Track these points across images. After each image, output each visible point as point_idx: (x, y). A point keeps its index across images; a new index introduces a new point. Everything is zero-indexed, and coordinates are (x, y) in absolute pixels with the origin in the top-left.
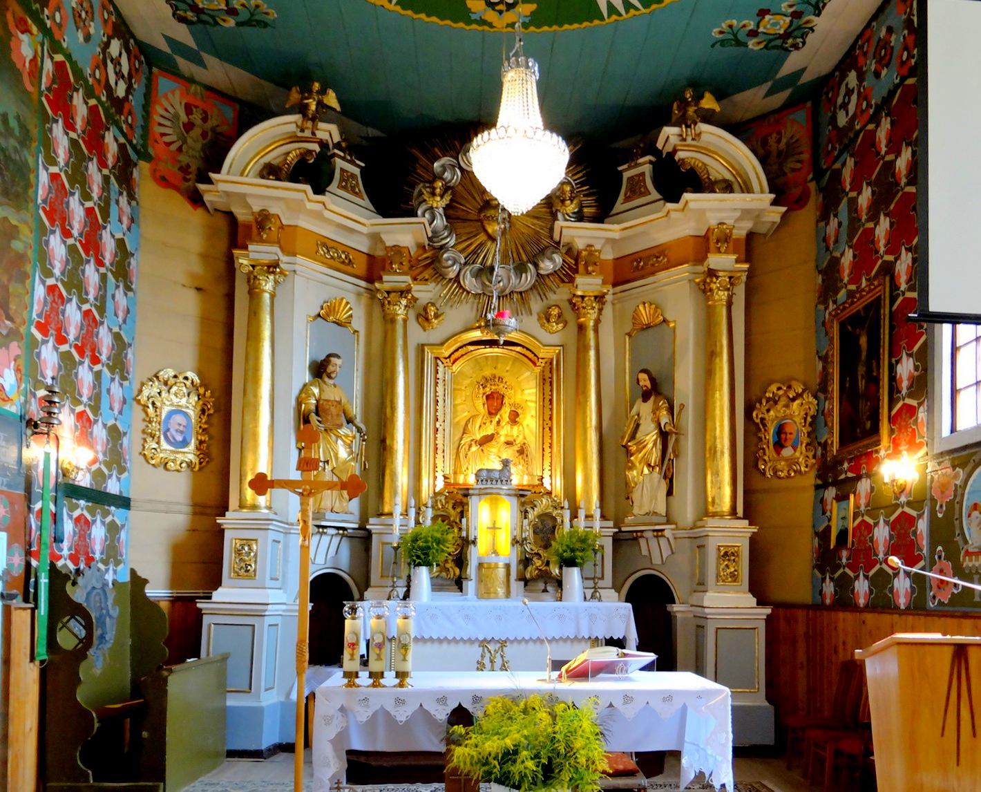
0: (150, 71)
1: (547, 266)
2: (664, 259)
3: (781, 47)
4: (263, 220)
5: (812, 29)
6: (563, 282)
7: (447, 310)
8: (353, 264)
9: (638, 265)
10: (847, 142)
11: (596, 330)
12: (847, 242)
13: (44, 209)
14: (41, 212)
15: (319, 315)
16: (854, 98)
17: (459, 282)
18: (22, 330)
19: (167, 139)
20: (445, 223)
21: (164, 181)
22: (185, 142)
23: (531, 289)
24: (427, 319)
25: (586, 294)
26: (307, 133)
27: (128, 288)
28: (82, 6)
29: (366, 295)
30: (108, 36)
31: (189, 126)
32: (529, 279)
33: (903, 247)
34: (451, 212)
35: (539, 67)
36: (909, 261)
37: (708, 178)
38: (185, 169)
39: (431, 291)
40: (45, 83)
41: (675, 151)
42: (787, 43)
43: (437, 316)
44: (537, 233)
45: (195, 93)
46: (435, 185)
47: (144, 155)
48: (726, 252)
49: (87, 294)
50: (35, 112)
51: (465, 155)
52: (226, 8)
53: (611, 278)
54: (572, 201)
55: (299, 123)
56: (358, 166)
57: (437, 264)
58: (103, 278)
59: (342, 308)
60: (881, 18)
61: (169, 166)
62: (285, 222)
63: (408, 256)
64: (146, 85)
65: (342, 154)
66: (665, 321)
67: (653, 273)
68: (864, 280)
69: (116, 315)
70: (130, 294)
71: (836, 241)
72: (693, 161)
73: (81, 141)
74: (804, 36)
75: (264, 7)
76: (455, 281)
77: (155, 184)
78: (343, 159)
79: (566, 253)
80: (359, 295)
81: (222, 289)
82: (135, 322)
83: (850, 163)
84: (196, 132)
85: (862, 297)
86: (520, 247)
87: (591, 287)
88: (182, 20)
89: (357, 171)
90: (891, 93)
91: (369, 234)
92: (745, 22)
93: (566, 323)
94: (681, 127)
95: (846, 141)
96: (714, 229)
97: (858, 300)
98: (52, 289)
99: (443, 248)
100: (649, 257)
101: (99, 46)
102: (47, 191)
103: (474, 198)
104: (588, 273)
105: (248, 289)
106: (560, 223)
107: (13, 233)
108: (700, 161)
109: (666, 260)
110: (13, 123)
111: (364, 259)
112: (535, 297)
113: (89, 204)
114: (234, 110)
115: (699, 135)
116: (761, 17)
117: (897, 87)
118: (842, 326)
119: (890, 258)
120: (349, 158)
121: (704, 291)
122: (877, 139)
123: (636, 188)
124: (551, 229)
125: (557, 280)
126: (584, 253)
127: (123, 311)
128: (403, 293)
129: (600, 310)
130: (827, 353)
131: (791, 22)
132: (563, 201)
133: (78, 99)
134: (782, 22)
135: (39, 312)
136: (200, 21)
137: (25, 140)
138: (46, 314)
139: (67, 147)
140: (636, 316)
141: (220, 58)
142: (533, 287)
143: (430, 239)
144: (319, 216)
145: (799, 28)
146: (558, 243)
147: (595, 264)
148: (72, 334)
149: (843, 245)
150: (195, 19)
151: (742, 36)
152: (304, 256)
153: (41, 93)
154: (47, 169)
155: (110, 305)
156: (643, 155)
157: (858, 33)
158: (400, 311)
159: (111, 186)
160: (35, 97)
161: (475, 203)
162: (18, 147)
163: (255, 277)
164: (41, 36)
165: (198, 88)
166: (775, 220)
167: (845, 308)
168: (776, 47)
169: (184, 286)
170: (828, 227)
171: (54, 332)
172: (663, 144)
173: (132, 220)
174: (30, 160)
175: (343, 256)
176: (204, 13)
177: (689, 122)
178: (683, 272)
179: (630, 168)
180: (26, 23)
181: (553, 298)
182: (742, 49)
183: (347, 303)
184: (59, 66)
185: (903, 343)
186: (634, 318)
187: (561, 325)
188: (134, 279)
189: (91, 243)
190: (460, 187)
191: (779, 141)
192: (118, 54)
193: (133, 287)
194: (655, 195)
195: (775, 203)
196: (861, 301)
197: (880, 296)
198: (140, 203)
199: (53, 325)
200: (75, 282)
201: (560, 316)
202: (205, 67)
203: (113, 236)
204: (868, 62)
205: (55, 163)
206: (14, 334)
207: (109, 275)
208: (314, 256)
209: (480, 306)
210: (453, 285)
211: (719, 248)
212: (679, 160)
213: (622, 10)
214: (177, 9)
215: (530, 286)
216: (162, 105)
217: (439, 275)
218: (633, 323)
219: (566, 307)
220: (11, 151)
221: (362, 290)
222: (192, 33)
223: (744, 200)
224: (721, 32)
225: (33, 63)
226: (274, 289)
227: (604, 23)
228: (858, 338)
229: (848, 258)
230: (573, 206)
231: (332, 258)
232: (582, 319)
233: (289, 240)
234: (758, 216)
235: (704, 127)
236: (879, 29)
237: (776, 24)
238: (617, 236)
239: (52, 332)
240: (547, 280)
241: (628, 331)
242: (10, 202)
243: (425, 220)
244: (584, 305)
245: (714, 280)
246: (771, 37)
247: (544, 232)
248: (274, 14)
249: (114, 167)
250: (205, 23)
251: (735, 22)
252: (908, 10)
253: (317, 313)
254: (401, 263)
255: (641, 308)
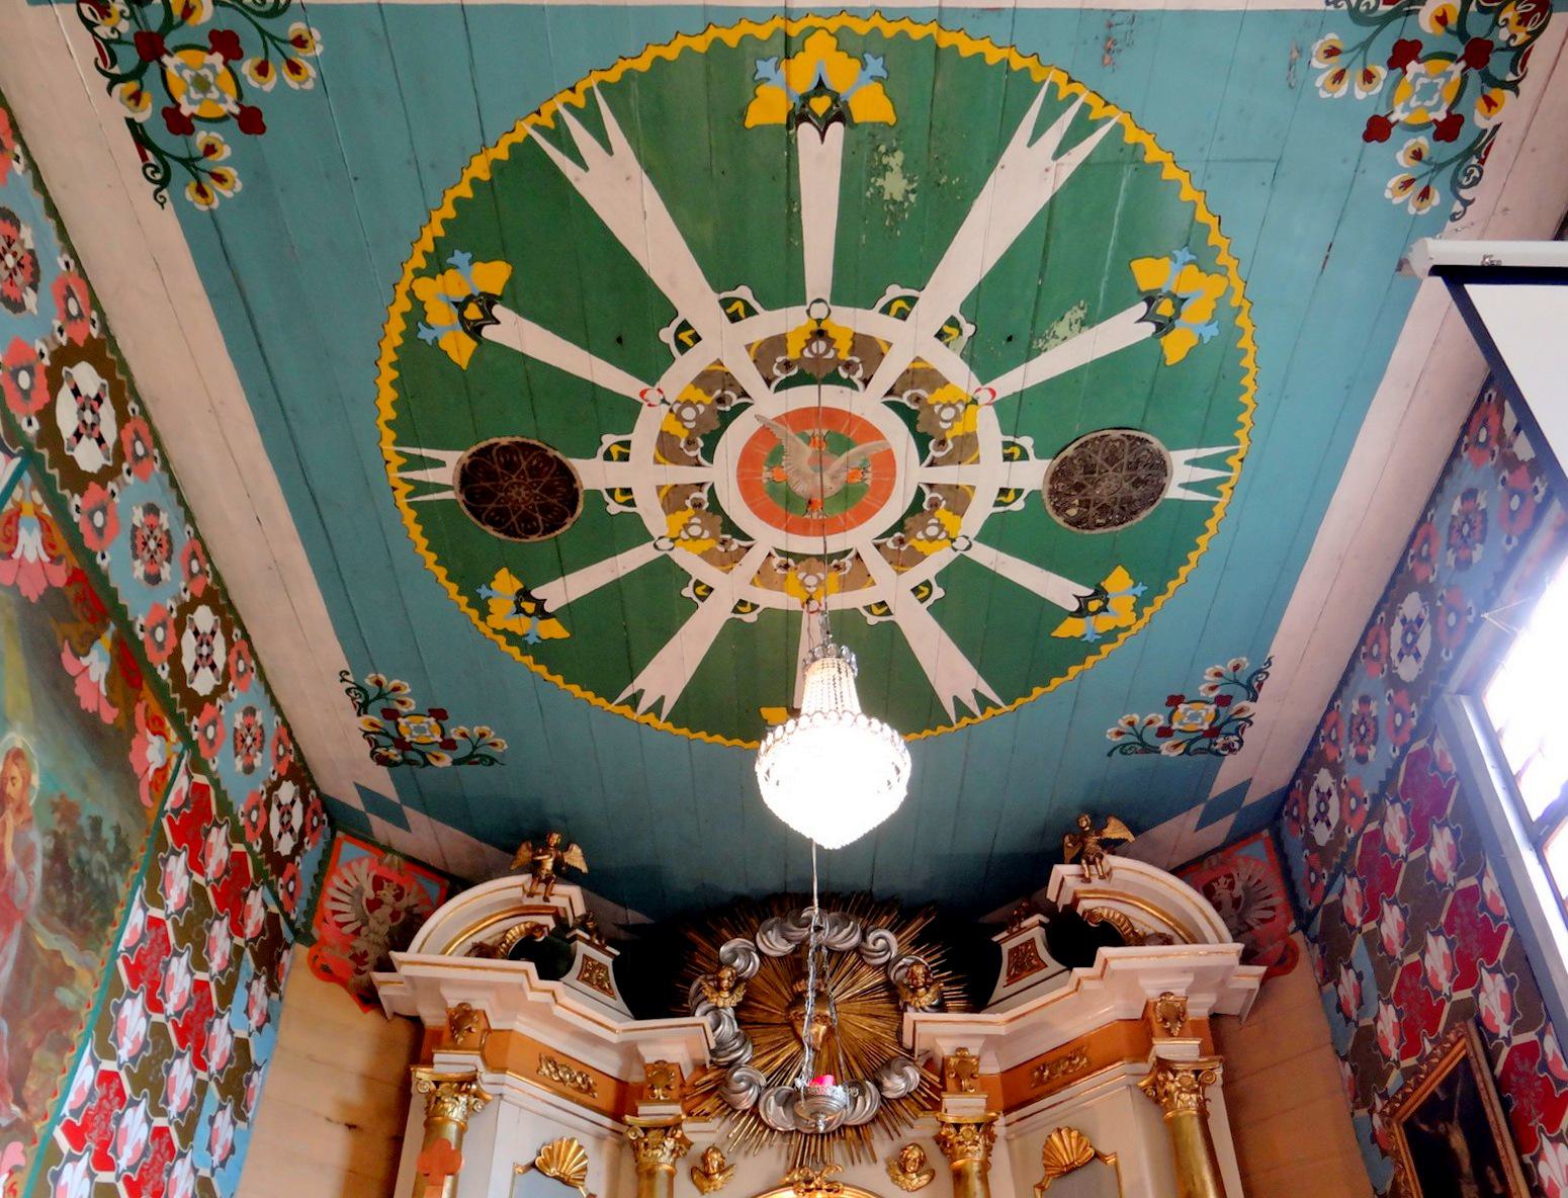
0: (333, 835)
1: (896, 1085)
2: (1081, 1060)
3: (1209, 750)
4: (461, 1018)
5: (1248, 720)
6: (924, 1109)
7: (740, 1160)
8: (594, 1091)
9: (1041, 1075)
10: (1339, 860)
11: (984, 1178)
12: (1379, 998)
13: (126, 961)
14: (120, 963)
15: (533, 1165)
16: (1334, 801)
17: (758, 1116)
18: (37, 1127)
19: (340, 918)
20: (737, 1030)
21: (325, 973)
22: (365, 923)
23: (872, 1121)
24: (707, 1175)
25: (962, 1121)
26: (537, 901)
27: (240, 1114)
28: (249, 730)
29: (610, 1138)
30: (279, 775)
31: (374, 904)
32: (868, 1104)
33: (1484, 972)
34: (745, 1014)
35: (857, 657)
36: (1503, 987)
37: (1133, 931)
38: (359, 958)
39: (713, 1132)
40: (173, 803)
41: (1076, 901)
42: (1216, 744)
43: (722, 1170)
44: (877, 1038)
45: (389, 866)
46: (721, 975)
47: (303, 935)
48: (1181, 1036)
49: (167, 1102)
50: (147, 832)
51: (765, 933)
52: (440, 740)
53: (1001, 1103)
54: (928, 990)
55: (527, 887)
56: (610, 954)
57: (724, 1089)
58: (201, 1088)
59: (570, 1155)
60: (1346, 693)
61: (337, 953)
62: (493, 1026)
63: (679, 1076)
64: (324, 851)
65: (587, 937)
66: (1097, 1155)
67: (1067, 1084)
68: (1426, 1043)
69: (210, 1148)
70: (241, 1125)
71: (1360, 1003)
72: (1106, 911)
73: (209, 890)
74: (1239, 731)
75: (491, 737)
76: (751, 1114)
77: (311, 974)
78: (589, 943)
79: (924, 1067)
80: (600, 1138)
81: (386, 1128)
82: (240, 1170)
83: (1353, 886)
84: (384, 912)
85: (1432, 1068)
86: (851, 1059)
87: (966, 1111)
88: (383, 761)
89: (608, 961)
90: (1392, 773)
91: (622, 1043)
92: (1151, 716)
93: (933, 1175)
94: (1079, 863)
95: (1336, 860)
96: (1156, 1003)
97: (1428, 1075)
98: (107, 1078)
99: (732, 1065)
100: (1057, 1063)
101: (264, 783)
102: (138, 937)
103: (779, 992)
104: (961, 1090)
105: (424, 1118)
106: (911, 1015)
107: (66, 975)
108: (1116, 911)
109: (1085, 1060)
110: (107, 833)
111: (611, 1086)
112: (878, 1133)
113: (201, 976)
114: (442, 887)
115: (1109, 873)
116: (1172, 708)
117: (1398, 762)
118: (1410, 1128)
119: (1466, 994)
120: (596, 942)
121: (1157, 1101)
122: (1387, 838)
123: (1025, 962)
124: (899, 1033)
125: (914, 1108)
126: (953, 1061)
127: (224, 1148)
128: (667, 1129)
129: (988, 1150)
130: (1395, 1184)
131: (1217, 711)
132: (914, 991)
133: (217, 839)
134: (1204, 713)
135: (75, 1107)
136: (408, 761)
137: (121, 859)
138: (87, 1114)
139: (185, 890)
140: (1048, 1150)
141: (427, 813)
142: (876, 1119)
143: (713, 1052)
144: (544, 1015)
145: (1229, 720)
146: (911, 1051)
147: (972, 1076)
148: (125, 1158)
149: (1374, 1004)
150: (399, 758)
151: (1150, 737)
152: (517, 1073)
153: (162, 813)
154: (145, 910)
155: (202, 1131)
156: (1027, 916)
157: (1318, 723)
158: (663, 1159)
159: (243, 963)
160: (152, 814)
161: (779, 999)
162: (108, 869)
163: (438, 1099)
164: (180, 747)
165: (396, 858)
166: (1252, 987)
167: (1406, 1097)
168: (1201, 751)
169: (328, 1120)
170: (1340, 986)
171: (94, 1146)
172: (1056, 893)
173: (267, 1018)
174: (122, 891)
175: (579, 1080)
176: (412, 749)
177: (1091, 858)
178: (1117, 1074)
179: (1012, 935)
180: (162, 724)
181: (908, 1134)
182: (1153, 755)
183: (580, 1147)
184: (197, 788)
185: (1536, 1123)
186: (1045, 1157)
187: (925, 1178)
188: (253, 1104)
189: (193, 1031)
190: (759, 979)
191: (1231, 886)
192: (289, 800)
193: (250, 1115)
194: (1054, 966)
195: (1247, 958)
196: (1434, 1075)
197: (1466, 1057)
198: (285, 1000)
199: (94, 1134)
200: (151, 1078)
201: (922, 1162)
202: (407, 828)
203: (231, 1032)
204: (1343, 750)
205: (161, 905)
206: (20, 1130)
207: (212, 1085)
208: (534, 1075)
209: (792, 1152)
210: (748, 1119)
211: (1169, 1030)
212: (1084, 913)
213: (975, 709)
214: (377, 746)
215: (870, 1115)
216: (341, 875)
217: (729, 1108)
218: (1046, 1166)
219: (933, 1150)
220: (94, 866)
221: (607, 1132)
222: (394, 779)
223: (1196, 954)
224: (1119, 733)
225: (161, 774)
226: (466, 1117)
227: (952, 729)
228: (1445, 1140)
229: (1388, 1021)
230: (929, 996)
231: (562, 1080)
232: (960, 1162)
233: (498, 1050)
234: (1223, 982)
235: (1112, 861)
236: (1348, 706)
237: (1196, 717)
238: (1002, 1030)
239: (91, 1144)
240: (898, 1107)
241: (1038, 1181)
242: (72, 934)
243: (708, 1020)
244: (961, 1138)
245: (1171, 1077)
246: (1193, 736)
247: (889, 1038)
248: (503, 745)
249: (255, 940)
250: (411, 762)
251: (1136, 717)
252: (1386, 666)
253: (530, 1160)
254: (668, 1087)
255: (1055, 1138)
